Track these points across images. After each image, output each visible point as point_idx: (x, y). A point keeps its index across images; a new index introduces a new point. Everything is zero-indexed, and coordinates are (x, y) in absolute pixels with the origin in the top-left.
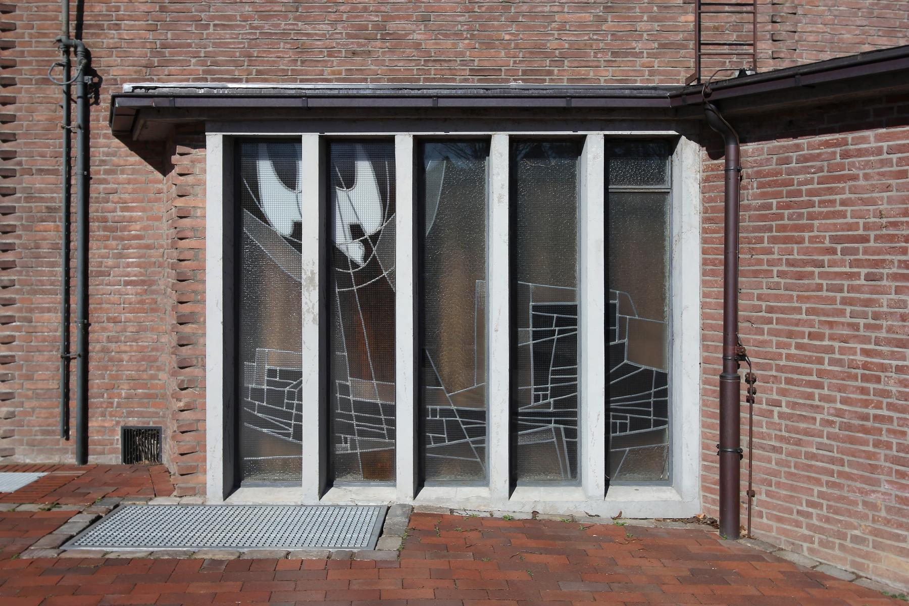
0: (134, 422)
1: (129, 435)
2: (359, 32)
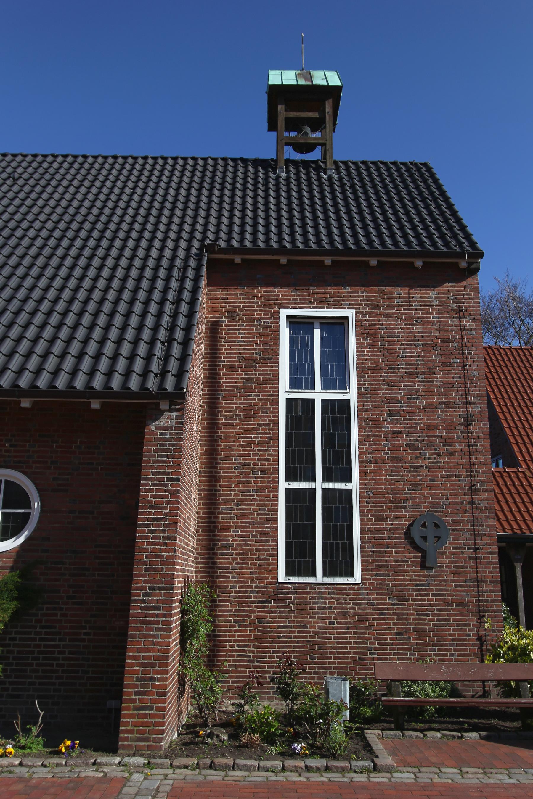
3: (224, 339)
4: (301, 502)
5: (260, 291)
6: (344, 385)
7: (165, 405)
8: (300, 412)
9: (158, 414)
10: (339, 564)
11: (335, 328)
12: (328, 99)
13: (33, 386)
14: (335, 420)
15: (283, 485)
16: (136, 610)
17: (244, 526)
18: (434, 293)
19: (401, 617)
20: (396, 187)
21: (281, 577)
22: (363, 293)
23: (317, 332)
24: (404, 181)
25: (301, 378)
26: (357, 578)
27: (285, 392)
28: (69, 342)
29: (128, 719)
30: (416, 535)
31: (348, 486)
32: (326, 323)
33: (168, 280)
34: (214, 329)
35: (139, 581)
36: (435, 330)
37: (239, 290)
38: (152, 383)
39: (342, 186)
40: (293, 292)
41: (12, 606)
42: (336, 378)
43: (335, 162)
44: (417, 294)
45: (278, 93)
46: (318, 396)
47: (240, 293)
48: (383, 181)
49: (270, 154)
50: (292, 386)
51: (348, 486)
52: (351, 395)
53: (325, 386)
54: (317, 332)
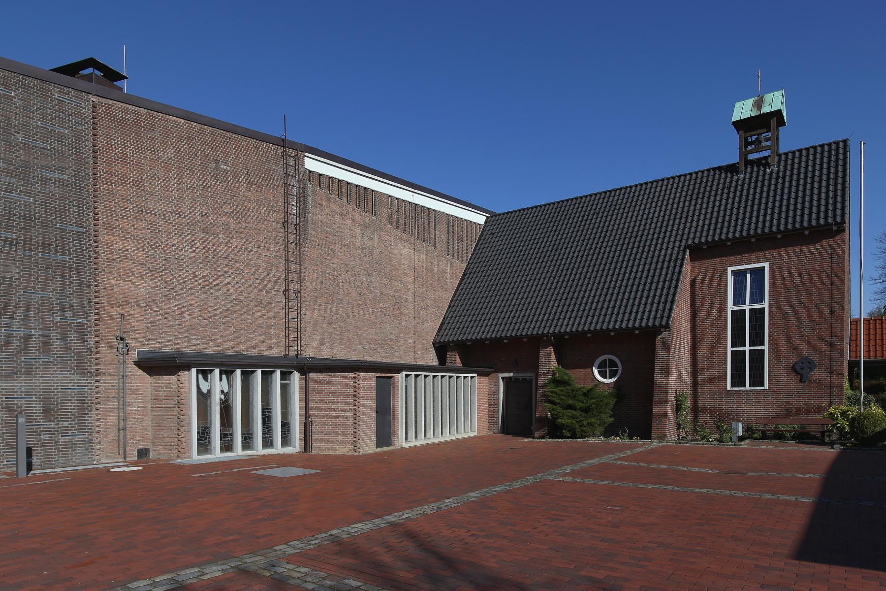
0: (141, 447)
1: (139, 451)
2: (205, 338)
3: (699, 286)
4: (738, 358)
5: (717, 260)
6: (761, 300)
7: (662, 330)
8: (738, 316)
9: (661, 333)
10: (757, 380)
11: (758, 274)
12: (772, 118)
13: (614, 328)
14: (757, 318)
15: (730, 349)
16: (656, 400)
17: (712, 367)
18: (816, 247)
19: (787, 403)
20: (789, 193)
21: (729, 388)
22: (773, 253)
23: (748, 276)
24: (821, 164)
25: (739, 299)
26: (766, 386)
27: (730, 307)
28: (681, 218)
29: (654, 431)
30: (798, 369)
31: (763, 347)
32: (753, 271)
33: (722, 195)
34: (693, 282)
35: (656, 391)
36: (815, 267)
37: (707, 261)
38: (657, 323)
39: (778, 178)
40: (735, 258)
41: (615, 400)
42: (757, 297)
43: (780, 156)
44: (805, 249)
45: (740, 125)
46: (748, 307)
47: (708, 263)
48: (806, 167)
49: (734, 158)
50: (734, 304)
51: (763, 347)
52: (766, 305)
53: (751, 302)
54: (748, 276)
